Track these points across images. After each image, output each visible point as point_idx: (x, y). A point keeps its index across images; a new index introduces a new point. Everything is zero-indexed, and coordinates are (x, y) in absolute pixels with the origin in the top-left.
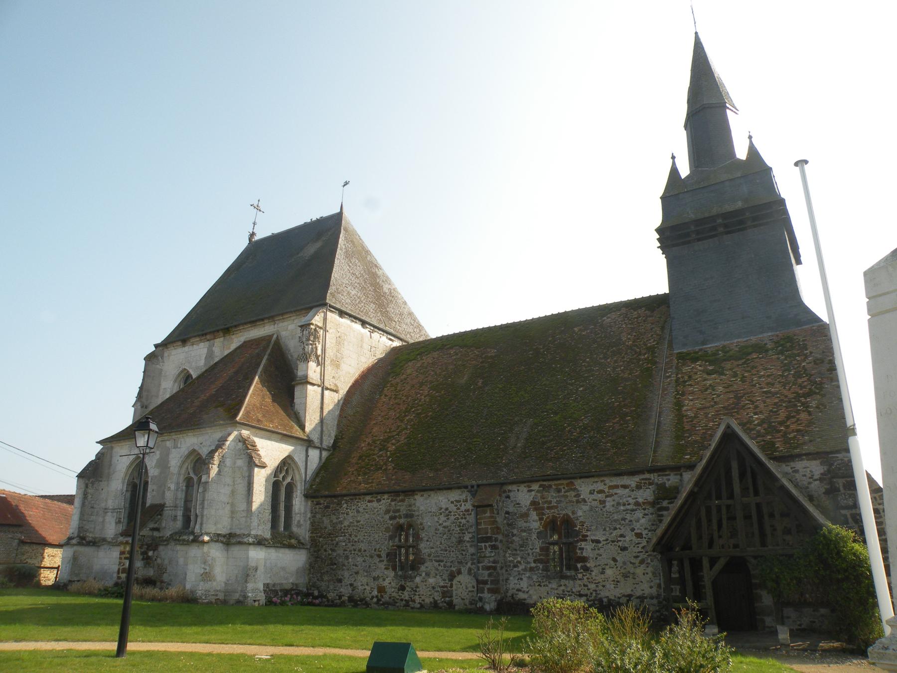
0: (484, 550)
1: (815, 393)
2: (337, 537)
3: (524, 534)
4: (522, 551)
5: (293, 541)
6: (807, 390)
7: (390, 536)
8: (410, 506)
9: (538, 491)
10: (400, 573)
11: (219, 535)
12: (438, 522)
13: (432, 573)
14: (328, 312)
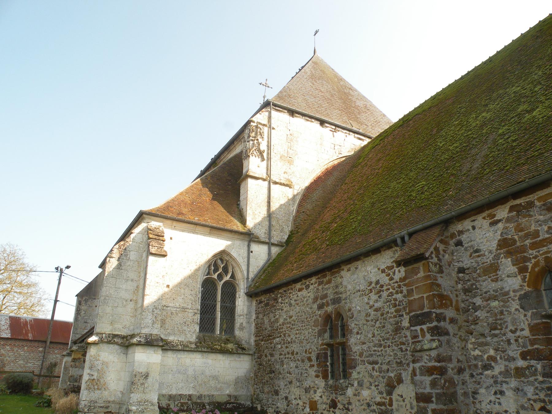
0: (420, 338)
2: (274, 338)
3: (495, 304)
4: (496, 336)
5: (230, 346)
8: (337, 287)
9: (508, 220)
10: (331, 382)
11: (115, 336)
12: (368, 303)
13: (366, 381)
14: (272, 111)
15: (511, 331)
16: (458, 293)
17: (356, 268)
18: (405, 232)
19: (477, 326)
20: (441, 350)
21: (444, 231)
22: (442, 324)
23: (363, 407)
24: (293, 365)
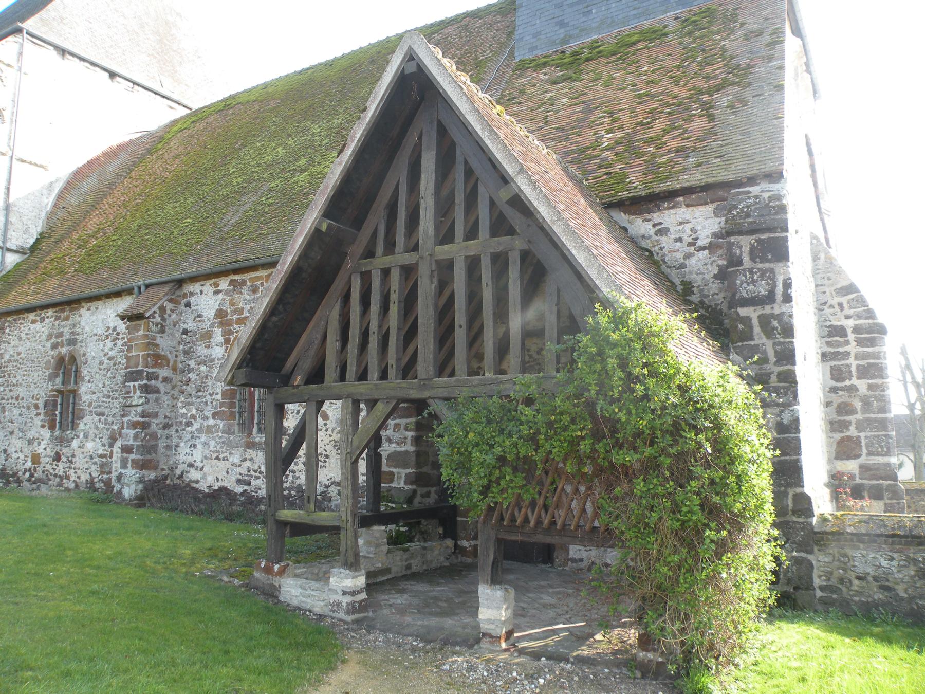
1: (733, 84)
3: (203, 368)
6: (718, 81)
7: (49, 374)
8: (74, 326)
9: (227, 293)
12: (103, 350)
13: (91, 432)
14: (25, 43)
15: (210, 394)
16: (178, 353)
17: (97, 309)
18: (142, 282)
19: (188, 387)
20: (146, 406)
21: (176, 290)
22: (153, 382)
23: (86, 459)
24: (16, 412)
